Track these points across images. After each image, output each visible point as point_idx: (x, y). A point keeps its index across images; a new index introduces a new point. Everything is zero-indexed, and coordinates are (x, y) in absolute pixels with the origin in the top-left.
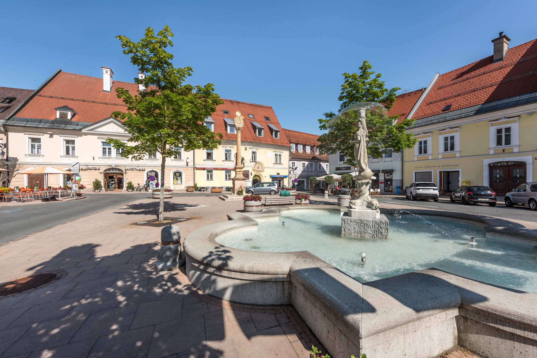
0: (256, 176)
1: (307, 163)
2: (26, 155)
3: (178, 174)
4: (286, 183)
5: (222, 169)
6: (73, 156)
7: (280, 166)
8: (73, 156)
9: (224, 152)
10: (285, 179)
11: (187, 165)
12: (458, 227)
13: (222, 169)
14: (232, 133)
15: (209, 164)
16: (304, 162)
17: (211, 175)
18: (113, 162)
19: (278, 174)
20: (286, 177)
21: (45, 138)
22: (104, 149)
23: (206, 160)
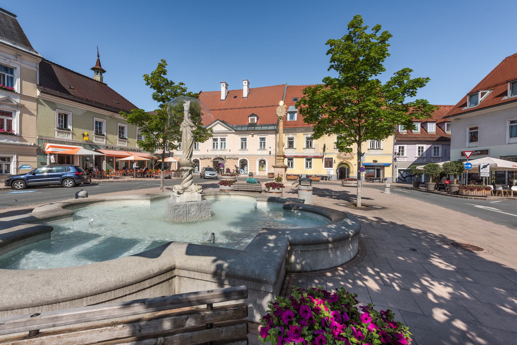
0: (342, 163)
1: (426, 147)
2: (368, 149)
3: (263, 162)
4: (388, 172)
5: (303, 157)
6: (198, 150)
7: (379, 152)
8: (198, 150)
9: (305, 140)
10: (386, 169)
11: (270, 153)
12: (245, 237)
13: (303, 157)
14: (292, 120)
15: (309, 152)
16: (421, 145)
17: (310, 163)
18: (218, 153)
19: (375, 161)
20: (388, 165)
21: (249, 137)
22: (214, 143)
23: (288, 148)
